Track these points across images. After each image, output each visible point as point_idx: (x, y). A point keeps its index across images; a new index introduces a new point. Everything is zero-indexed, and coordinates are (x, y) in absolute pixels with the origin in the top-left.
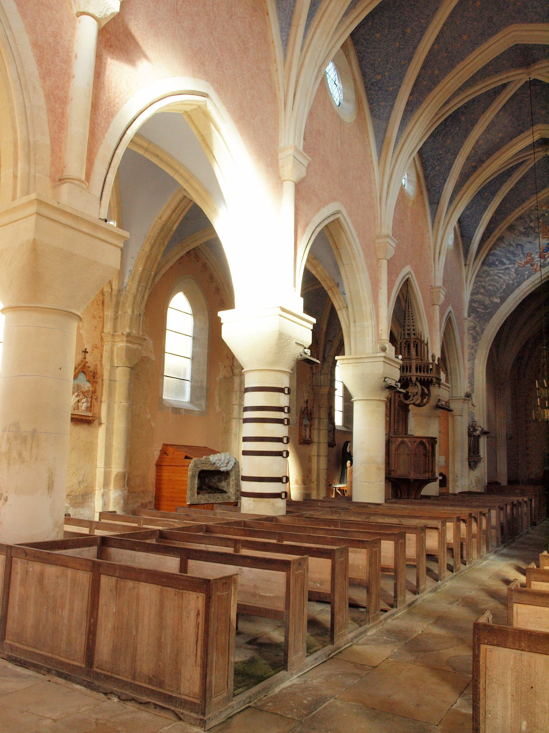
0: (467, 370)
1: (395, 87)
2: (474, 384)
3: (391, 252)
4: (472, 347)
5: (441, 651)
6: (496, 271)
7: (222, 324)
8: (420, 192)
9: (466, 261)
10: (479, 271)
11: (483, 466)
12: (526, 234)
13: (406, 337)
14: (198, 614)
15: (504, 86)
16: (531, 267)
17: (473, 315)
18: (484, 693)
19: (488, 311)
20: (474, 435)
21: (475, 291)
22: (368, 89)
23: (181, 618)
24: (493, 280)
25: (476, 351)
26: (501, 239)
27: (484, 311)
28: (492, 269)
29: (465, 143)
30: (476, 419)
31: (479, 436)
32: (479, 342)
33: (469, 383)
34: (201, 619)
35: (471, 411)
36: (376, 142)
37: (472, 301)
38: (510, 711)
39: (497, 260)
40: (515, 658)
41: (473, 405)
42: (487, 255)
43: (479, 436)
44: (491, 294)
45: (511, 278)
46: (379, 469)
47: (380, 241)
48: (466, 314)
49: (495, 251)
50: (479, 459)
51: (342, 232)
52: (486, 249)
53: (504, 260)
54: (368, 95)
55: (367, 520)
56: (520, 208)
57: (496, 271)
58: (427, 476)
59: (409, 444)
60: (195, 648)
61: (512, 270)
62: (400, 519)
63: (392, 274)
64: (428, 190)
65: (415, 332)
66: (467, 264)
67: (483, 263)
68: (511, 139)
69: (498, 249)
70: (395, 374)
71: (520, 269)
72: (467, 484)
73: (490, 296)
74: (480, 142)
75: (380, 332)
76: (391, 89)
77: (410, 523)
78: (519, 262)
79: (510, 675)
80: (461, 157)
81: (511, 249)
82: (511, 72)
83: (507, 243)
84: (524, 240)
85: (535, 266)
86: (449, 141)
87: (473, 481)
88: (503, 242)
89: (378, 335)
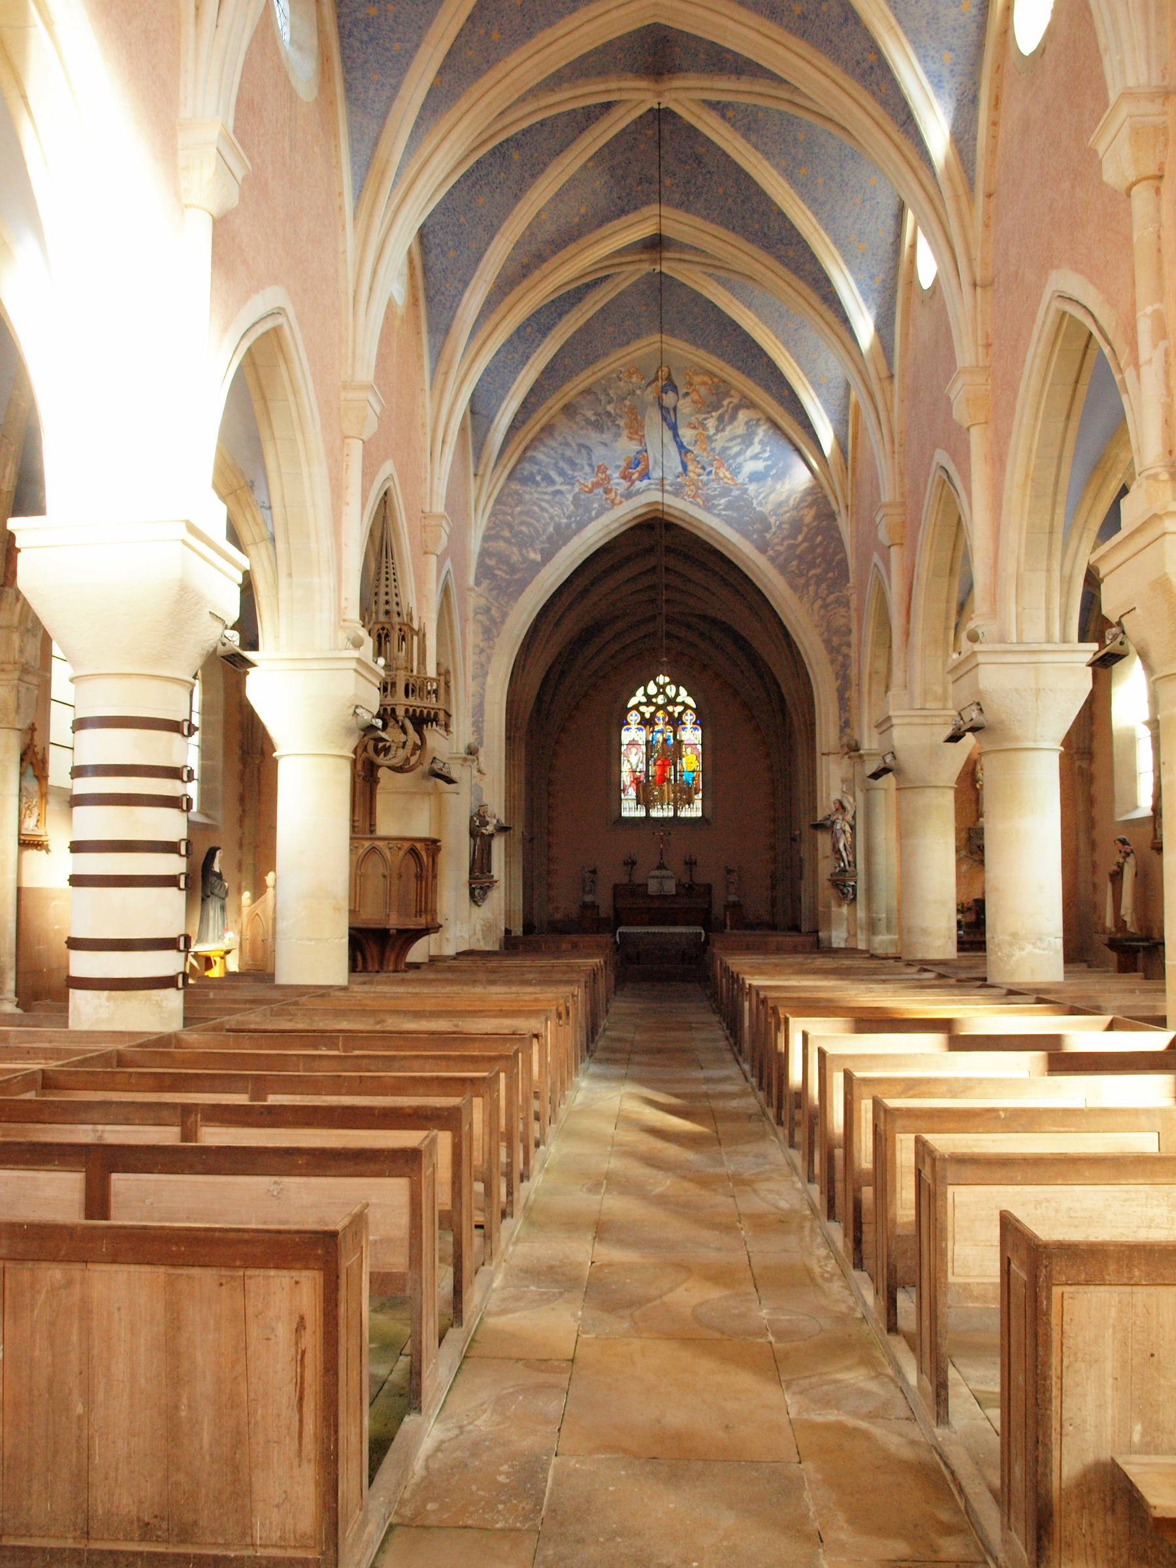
0: (471, 699)
1: (408, 46)
2: (482, 728)
3: (371, 427)
4: (482, 651)
5: (666, 1298)
6: (536, 495)
7: (19, 550)
8: (414, 301)
9: (477, 467)
10: (502, 490)
11: (497, 899)
12: (598, 426)
13: (382, 618)
14: (301, 1326)
15: (608, 106)
16: (604, 496)
17: (486, 583)
18: (1059, 1386)
19: (516, 577)
20: (483, 833)
21: (493, 532)
22: (345, 34)
23: (243, 1346)
24: (528, 513)
25: (489, 659)
26: (548, 429)
27: (508, 577)
28: (528, 489)
29: (514, 212)
30: (485, 800)
31: (492, 836)
32: (496, 640)
33: (473, 725)
34: (312, 1340)
35: (476, 784)
36: (353, 163)
37: (484, 553)
38: (1110, 1411)
39: (539, 472)
40: (1120, 1302)
41: (479, 771)
42: (520, 460)
43: (492, 836)
44: (523, 543)
45: (564, 514)
46: (337, 909)
47: (352, 395)
48: (471, 580)
49: (535, 454)
50: (491, 883)
51: (281, 362)
52: (518, 446)
53: (554, 474)
54: (343, 48)
55: (378, 1027)
56: (589, 372)
57: (536, 495)
58: (422, 922)
59: (387, 853)
60: (297, 1418)
61: (567, 496)
62: (455, 1021)
63: (368, 474)
64: (429, 300)
65: (399, 609)
66: (480, 472)
67: (510, 477)
68: (600, 225)
69: (542, 449)
70: (373, 700)
71: (583, 497)
72: (466, 936)
73: (521, 545)
74: (543, 216)
75: (344, 604)
76: (397, 46)
77: (480, 1026)
78: (582, 481)
79: (1110, 1341)
80: (504, 240)
81: (568, 453)
82: (626, 80)
83: (560, 439)
84: (593, 438)
85: (613, 494)
86: (481, 201)
87: (478, 928)
88: (551, 435)
89: (340, 611)
